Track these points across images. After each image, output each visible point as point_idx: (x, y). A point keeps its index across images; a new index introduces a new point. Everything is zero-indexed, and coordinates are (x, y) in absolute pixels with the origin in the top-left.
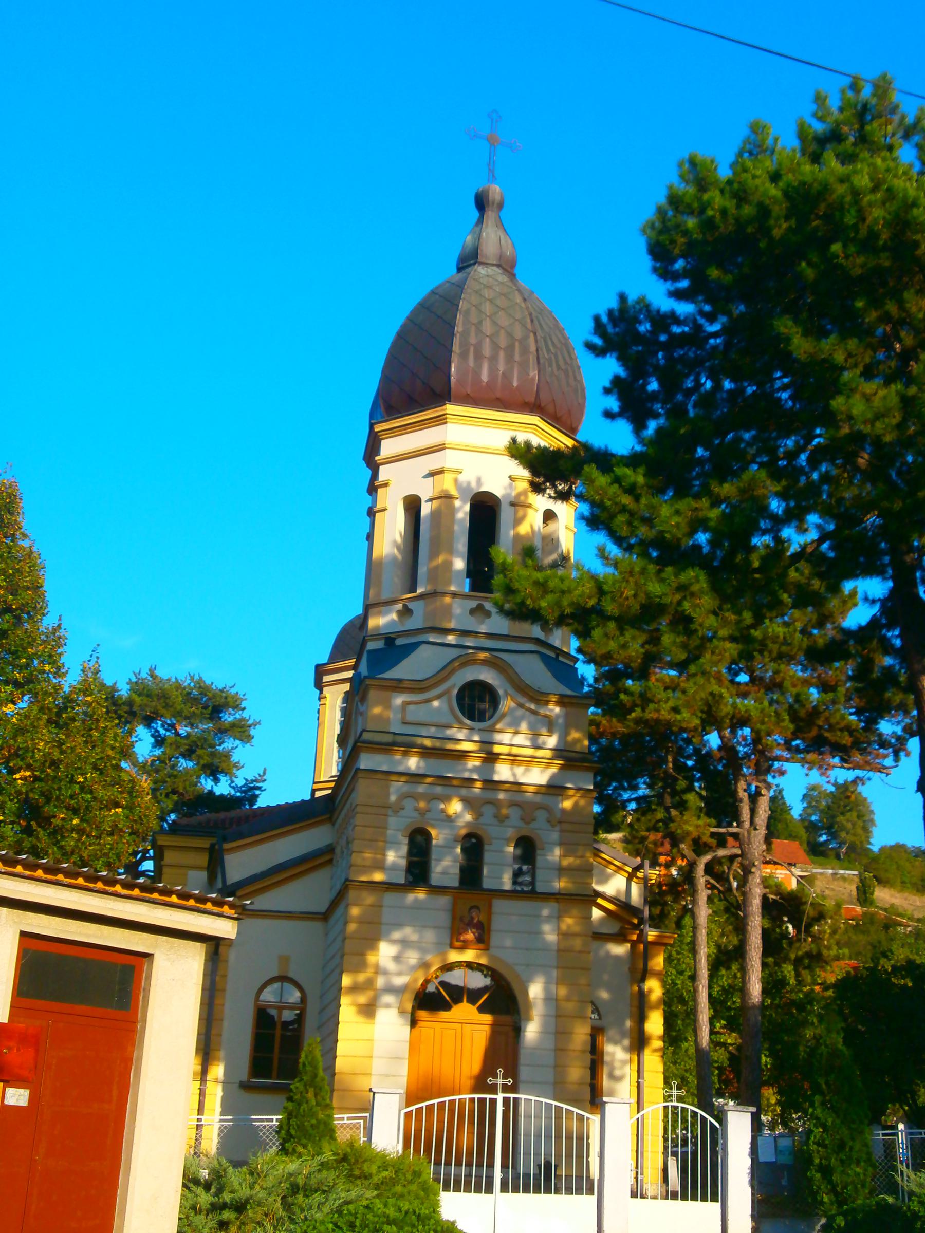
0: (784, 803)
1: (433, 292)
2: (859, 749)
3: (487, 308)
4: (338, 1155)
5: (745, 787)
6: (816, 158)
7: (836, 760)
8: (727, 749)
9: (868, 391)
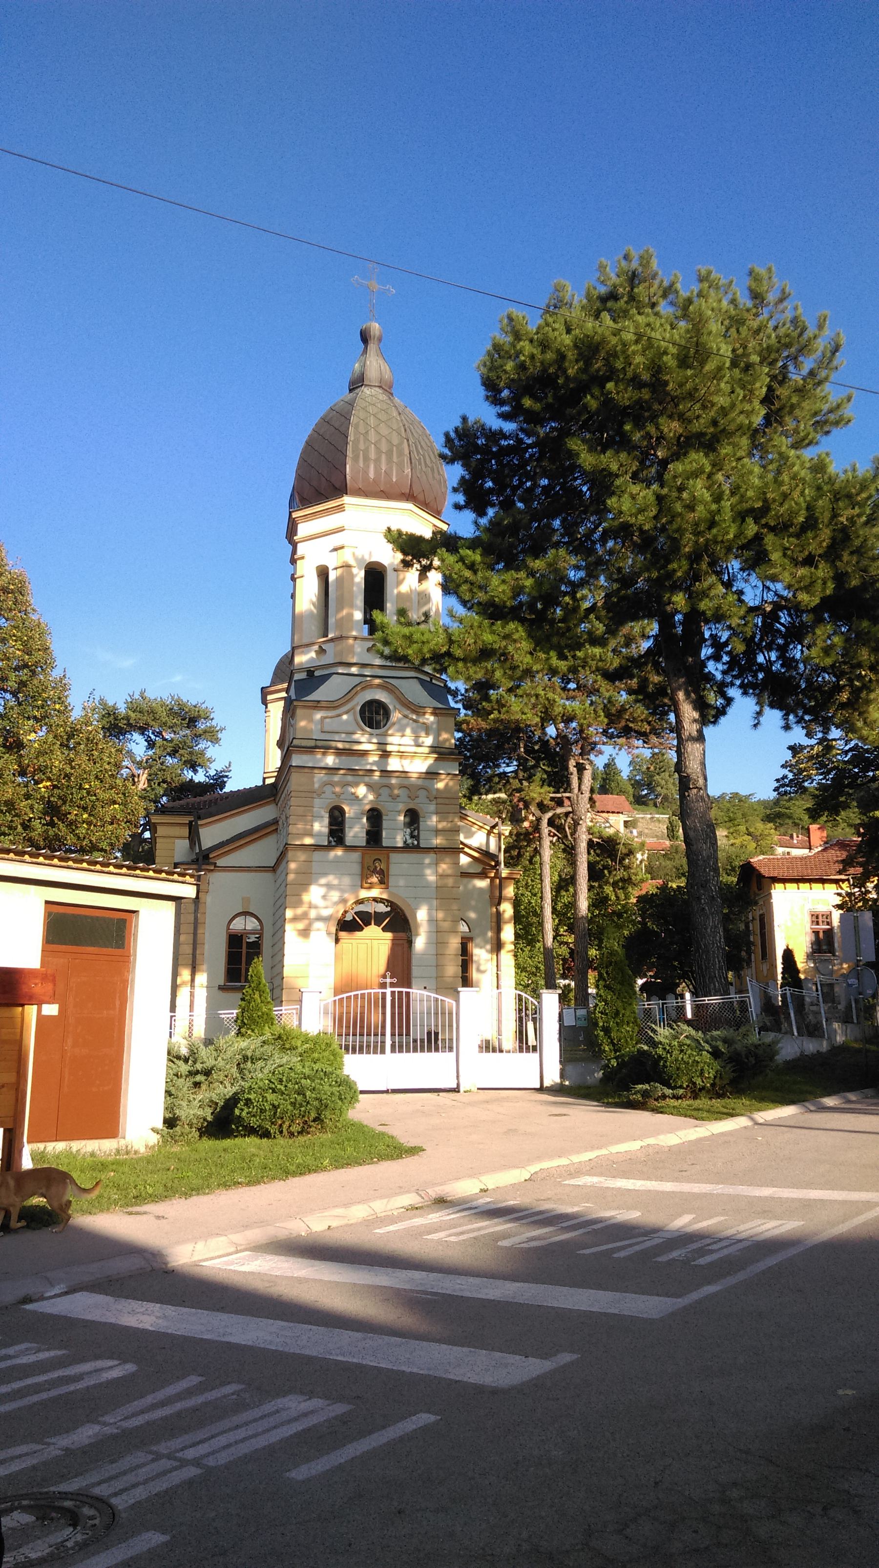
0: (616, 768)
2: (655, 734)
3: (372, 421)
6: (597, 316)
7: (641, 742)
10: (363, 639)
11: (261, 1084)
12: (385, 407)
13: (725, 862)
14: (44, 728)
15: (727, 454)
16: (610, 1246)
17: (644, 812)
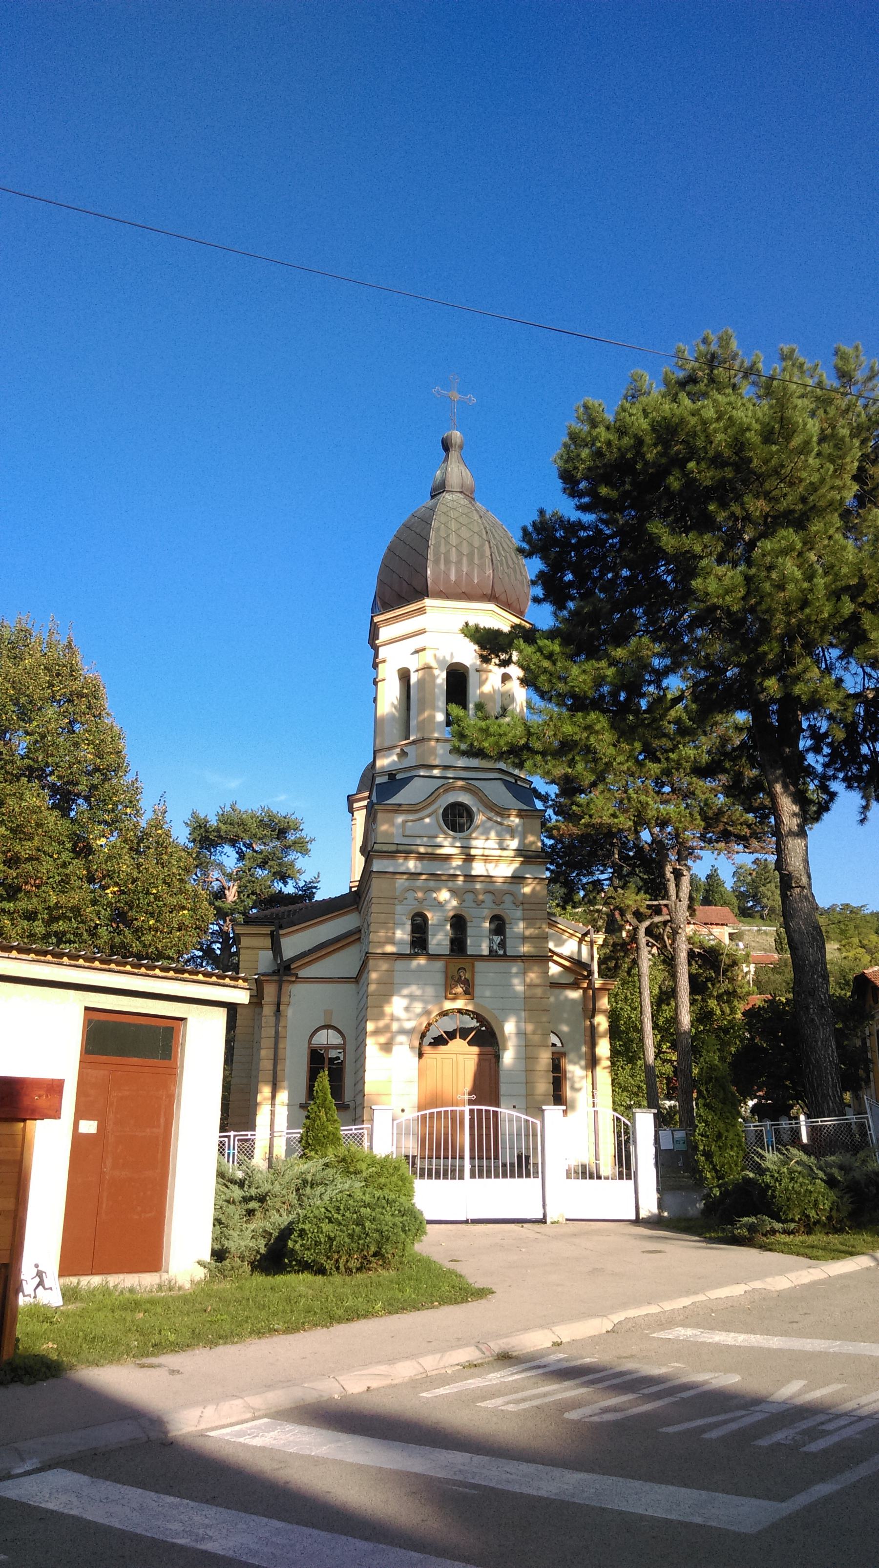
2: (756, 838)
3: (453, 525)
6: (675, 400)
7: (741, 847)
10: (446, 741)
11: (316, 1212)
12: (466, 510)
13: (838, 975)
14: (115, 834)
15: (818, 532)
16: (699, 1422)
17: (749, 924)
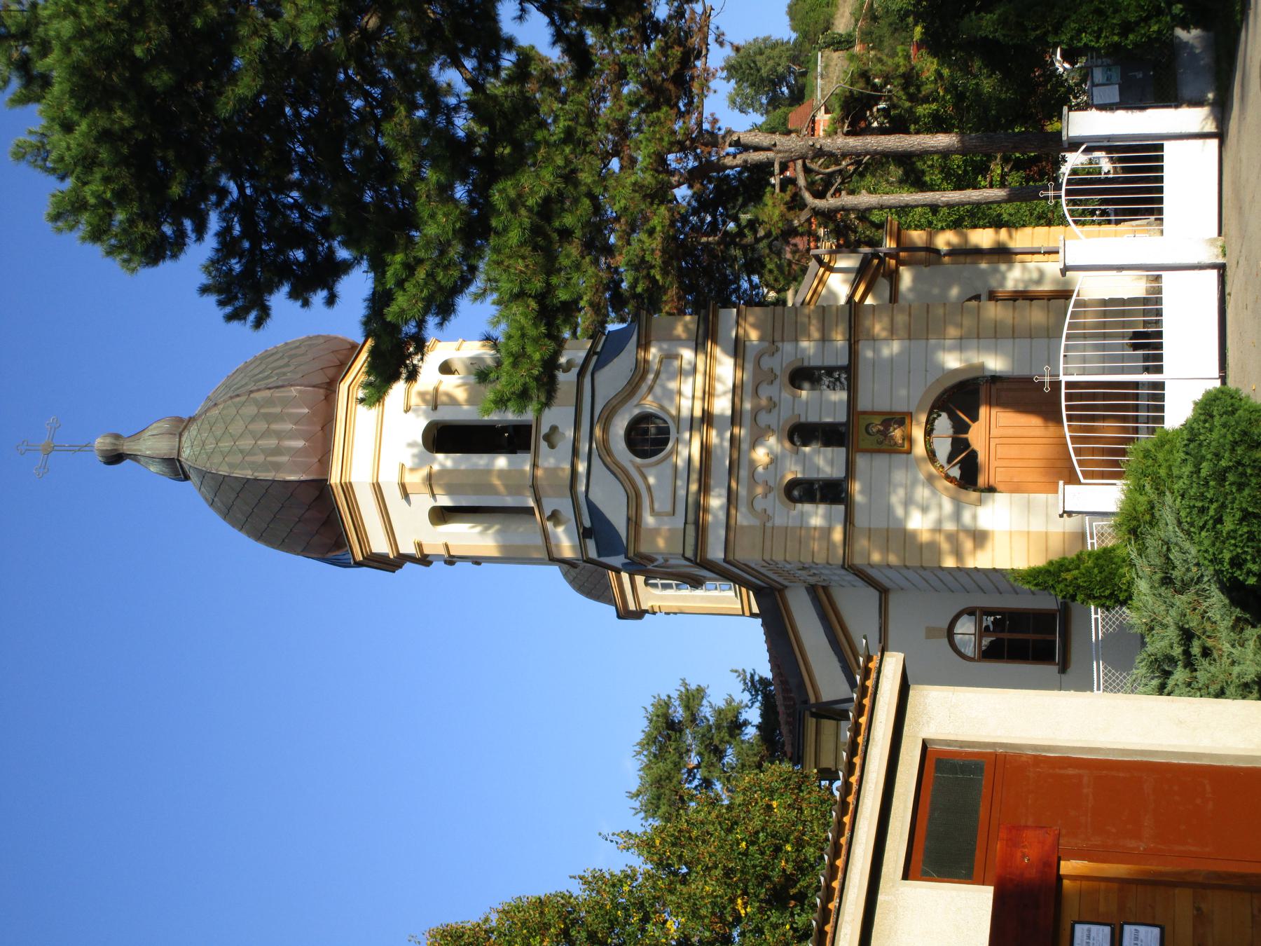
1: (212, 504)
2: (686, 39)
3: (225, 445)
4: (1129, 539)
5: (731, 158)
7: (698, 63)
8: (691, 177)
9: (293, 12)
11: (1207, 543)
17: (813, 91)
